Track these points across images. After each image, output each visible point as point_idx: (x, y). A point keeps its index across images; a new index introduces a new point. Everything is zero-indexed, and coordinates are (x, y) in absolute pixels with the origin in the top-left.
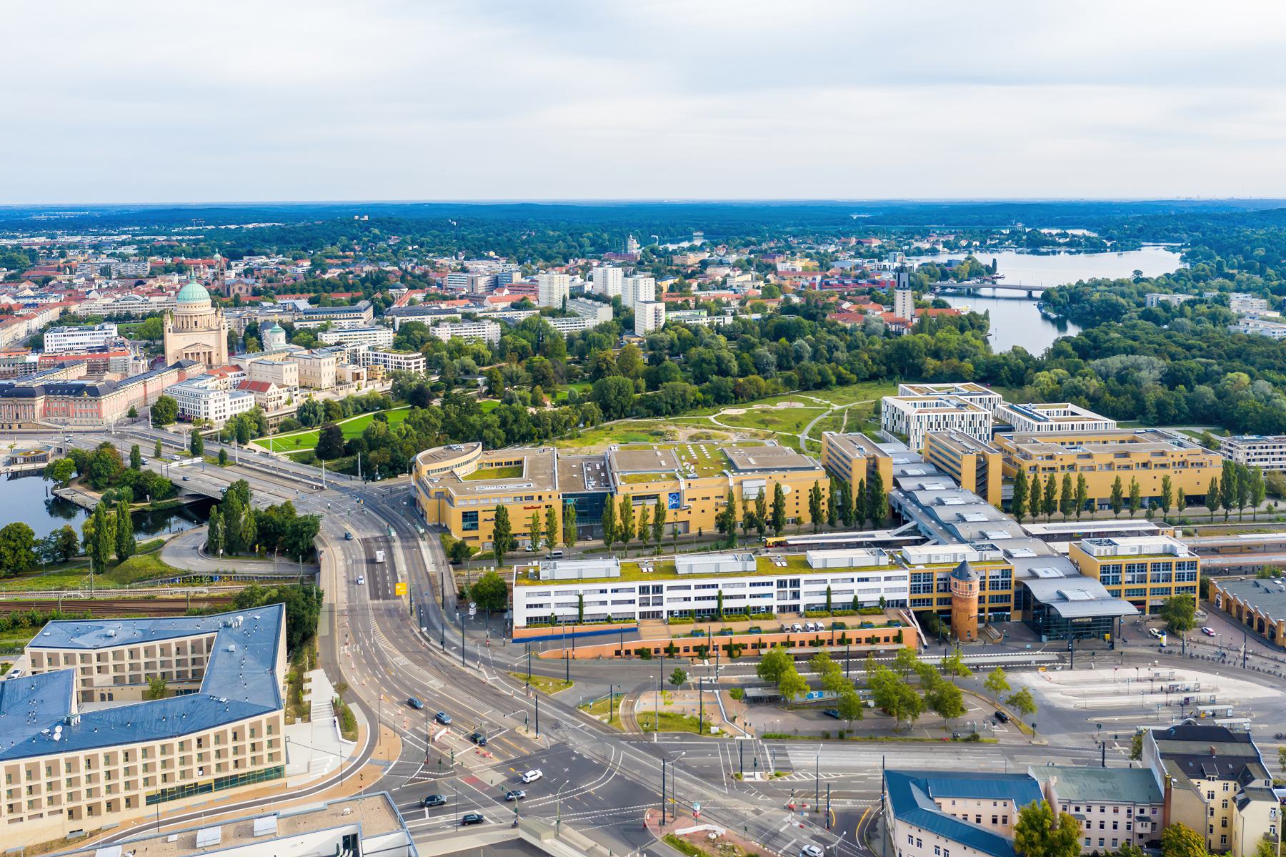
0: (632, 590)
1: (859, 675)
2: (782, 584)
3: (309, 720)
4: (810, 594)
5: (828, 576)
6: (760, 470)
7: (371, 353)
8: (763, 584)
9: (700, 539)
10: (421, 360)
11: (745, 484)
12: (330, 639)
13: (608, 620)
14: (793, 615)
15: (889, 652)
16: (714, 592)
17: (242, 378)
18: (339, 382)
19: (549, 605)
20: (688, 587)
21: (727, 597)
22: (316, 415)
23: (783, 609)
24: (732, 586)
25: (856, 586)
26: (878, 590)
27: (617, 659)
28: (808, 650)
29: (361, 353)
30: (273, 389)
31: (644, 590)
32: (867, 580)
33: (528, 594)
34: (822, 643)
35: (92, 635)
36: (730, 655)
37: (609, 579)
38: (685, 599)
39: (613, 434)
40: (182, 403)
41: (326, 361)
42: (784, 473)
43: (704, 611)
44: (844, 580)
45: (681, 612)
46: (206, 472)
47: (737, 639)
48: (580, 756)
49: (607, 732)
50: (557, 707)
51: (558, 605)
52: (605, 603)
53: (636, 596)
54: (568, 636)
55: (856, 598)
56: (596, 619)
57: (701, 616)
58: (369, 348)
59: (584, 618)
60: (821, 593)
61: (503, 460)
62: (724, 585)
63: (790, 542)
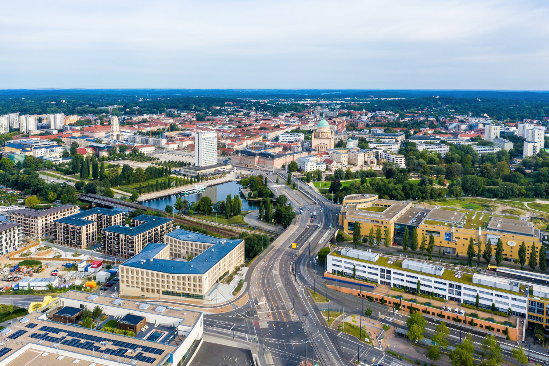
0: (377, 269)
1: (431, 331)
2: (451, 286)
3: (229, 284)
4: (467, 294)
5: (478, 289)
6: (500, 231)
7: (384, 153)
8: (441, 283)
9: (457, 258)
10: (403, 159)
11: (488, 236)
12: (261, 258)
13: (366, 280)
14: (456, 303)
15: (438, 322)
16: (415, 280)
17: (328, 158)
18: (366, 163)
19: (341, 267)
20: (403, 275)
21: (422, 285)
22: (340, 175)
23: (451, 299)
24: (425, 280)
25: (494, 298)
26: (508, 304)
27: (358, 298)
28: (436, 318)
29: (380, 153)
30: (334, 163)
31: (383, 271)
32: (501, 296)
33: (333, 260)
34: (460, 321)
35: (185, 236)
36: (411, 312)
37: (370, 262)
38: (402, 280)
39: (463, 202)
40: (299, 165)
41: (360, 154)
42: (513, 235)
43: (411, 288)
44: (487, 293)
45: (399, 286)
46: (286, 190)
47: (415, 305)
48: (302, 330)
49: (322, 324)
50: (314, 308)
51: (345, 268)
52: (365, 272)
53: (379, 272)
54: (338, 281)
55: (493, 304)
56: (361, 278)
57: (408, 290)
58: (384, 151)
59: (355, 276)
60: (473, 296)
61: (383, 204)
62: (421, 279)
63: (497, 270)
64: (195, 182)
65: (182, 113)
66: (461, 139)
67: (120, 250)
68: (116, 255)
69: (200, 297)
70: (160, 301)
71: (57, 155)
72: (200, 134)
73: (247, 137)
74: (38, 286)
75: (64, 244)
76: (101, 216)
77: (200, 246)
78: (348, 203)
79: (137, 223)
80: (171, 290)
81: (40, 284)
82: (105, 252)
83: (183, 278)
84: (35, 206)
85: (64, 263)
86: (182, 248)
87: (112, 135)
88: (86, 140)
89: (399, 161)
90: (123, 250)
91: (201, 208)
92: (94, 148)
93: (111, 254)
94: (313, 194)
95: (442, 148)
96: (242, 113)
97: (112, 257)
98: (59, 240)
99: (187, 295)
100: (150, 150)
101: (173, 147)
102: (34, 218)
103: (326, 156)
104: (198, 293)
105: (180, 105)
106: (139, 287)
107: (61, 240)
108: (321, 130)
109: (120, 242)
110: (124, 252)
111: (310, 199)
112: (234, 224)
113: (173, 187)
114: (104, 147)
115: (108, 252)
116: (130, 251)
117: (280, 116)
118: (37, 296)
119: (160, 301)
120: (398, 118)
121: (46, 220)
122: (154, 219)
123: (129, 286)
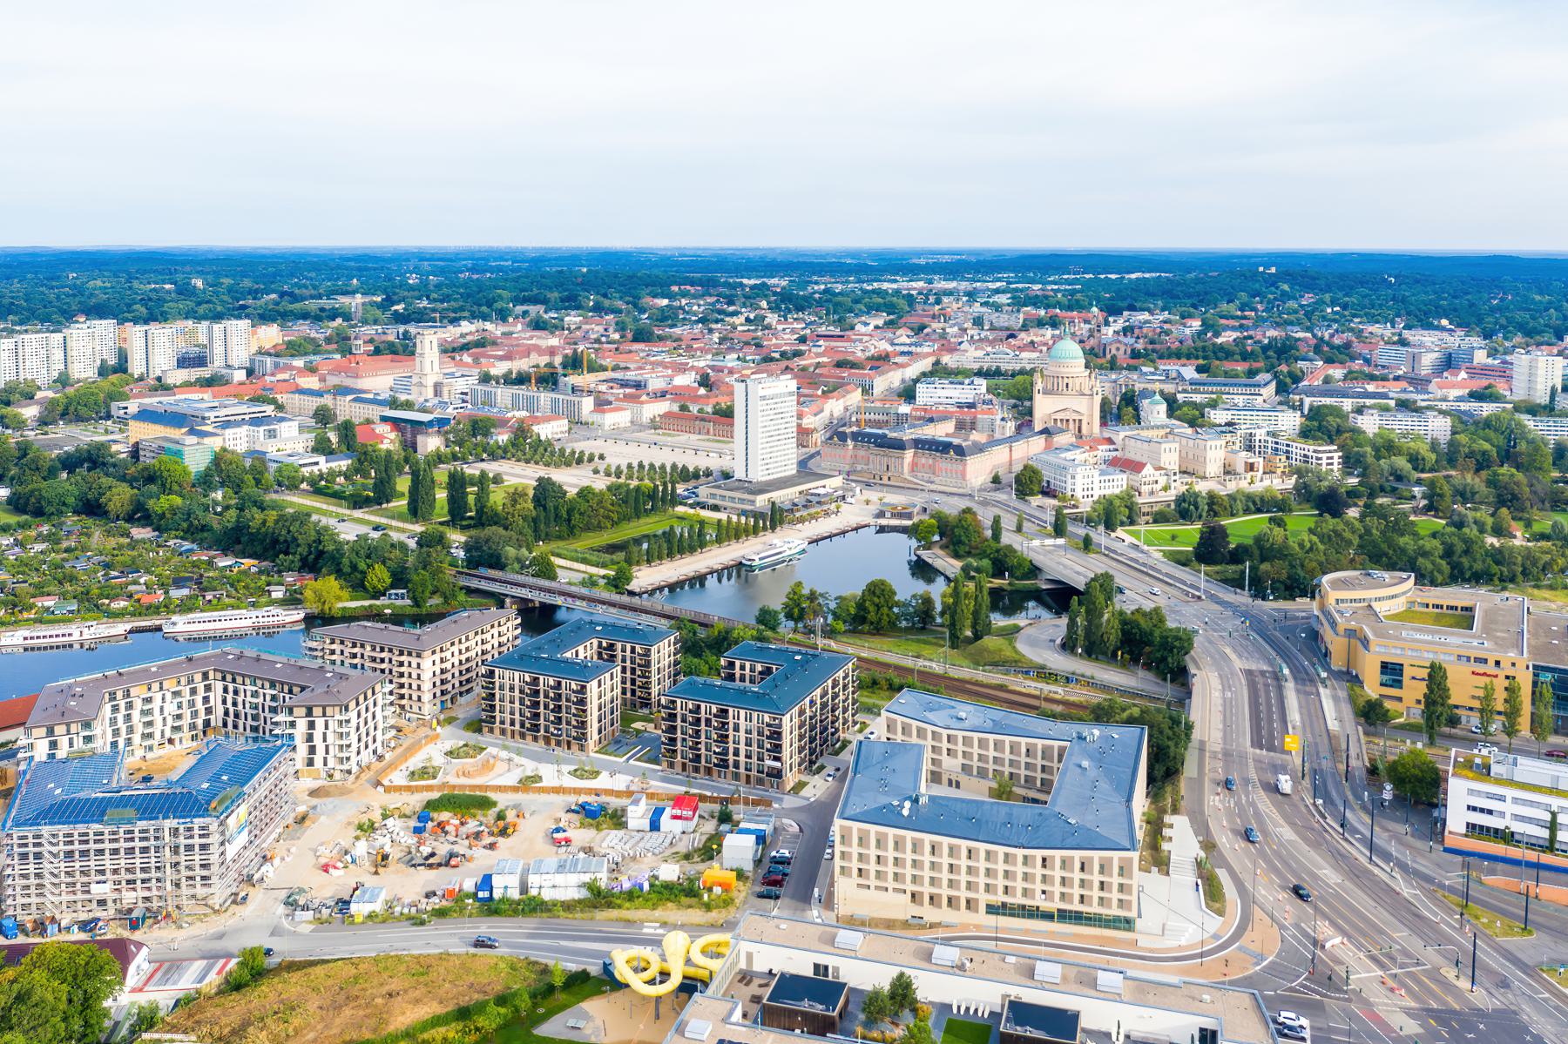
7: (1270, 439)
10: (1336, 455)
17: (1114, 454)
18: (1228, 471)
22: (1197, 508)
29: (1257, 438)
33: (1471, 792)
40: (1047, 475)
41: (1213, 443)
46: (1068, 556)
58: (1268, 433)
61: (1445, 603)
64: (765, 529)
65: (567, 319)
66: (1439, 394)
67: (731, 758)
68: (715, 775)
69: (1127, 924)
70: (996, 939)
71: (297, 446)
72: (223, 364)
73: (823, 392)
74: (554, 887)
75: (523, 736)
76: (611, 647)
77: (1014, 748)
78: (1342, 601)
79: (743, 668)
80: (1018, 899)
81: (559, 879)
82: (671, 765)
83: (914, 845)
84: (336, 613)
85: (572, 800)
86: (945, 752)
87: (421, 384)
88: (355, 400)
89: (1324, 461)
90: (742, 758)
91: (872, 616)
92: (396, 423)
93: (697, 770)
94: (1151, 562)
95: (1430, 424)
96: (742, 319)
97: (701, 778)
98: (502, 722)
99: (1064, 916)
100: (556, 430)
101: (617, 420)
102: (410, 654)
103: (1108, 447)
104: (1115, 911)
105: (554, 295)
106: (905, 892)
107: (512, 724)
108: (1062, 369)
109: (731, 733)
110: (742, 766)
111: (1171, 585)
112: (995, 664)
113: (711, 542)
114: (430, 424)
115: (684, 765)
116: (769, 763)
117: (859, 327)
118: (567, 921)
119: (996, 939)
120: (1200, 334)
121: (442, 661)
122: (798, 657)
123: (869, 887)
